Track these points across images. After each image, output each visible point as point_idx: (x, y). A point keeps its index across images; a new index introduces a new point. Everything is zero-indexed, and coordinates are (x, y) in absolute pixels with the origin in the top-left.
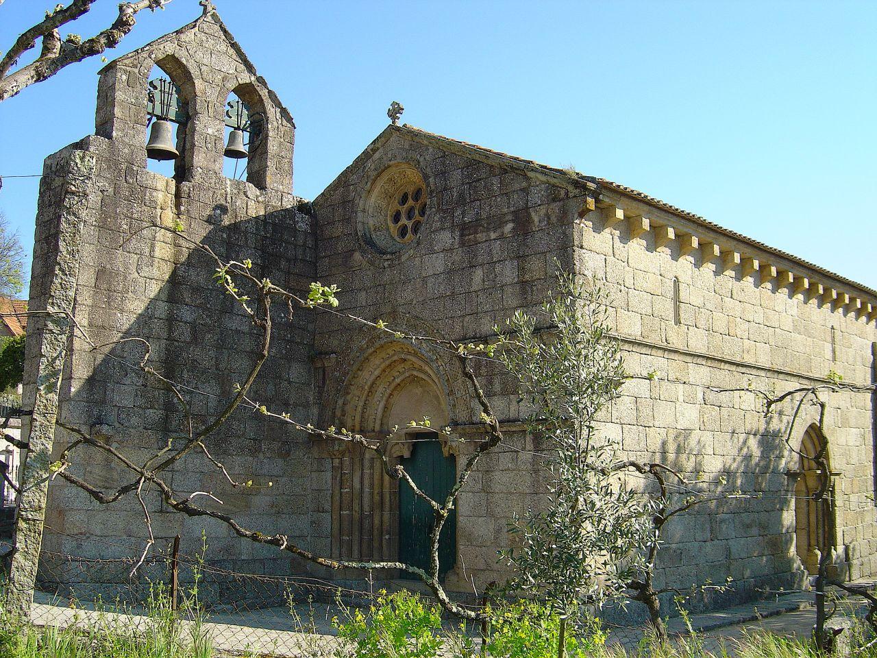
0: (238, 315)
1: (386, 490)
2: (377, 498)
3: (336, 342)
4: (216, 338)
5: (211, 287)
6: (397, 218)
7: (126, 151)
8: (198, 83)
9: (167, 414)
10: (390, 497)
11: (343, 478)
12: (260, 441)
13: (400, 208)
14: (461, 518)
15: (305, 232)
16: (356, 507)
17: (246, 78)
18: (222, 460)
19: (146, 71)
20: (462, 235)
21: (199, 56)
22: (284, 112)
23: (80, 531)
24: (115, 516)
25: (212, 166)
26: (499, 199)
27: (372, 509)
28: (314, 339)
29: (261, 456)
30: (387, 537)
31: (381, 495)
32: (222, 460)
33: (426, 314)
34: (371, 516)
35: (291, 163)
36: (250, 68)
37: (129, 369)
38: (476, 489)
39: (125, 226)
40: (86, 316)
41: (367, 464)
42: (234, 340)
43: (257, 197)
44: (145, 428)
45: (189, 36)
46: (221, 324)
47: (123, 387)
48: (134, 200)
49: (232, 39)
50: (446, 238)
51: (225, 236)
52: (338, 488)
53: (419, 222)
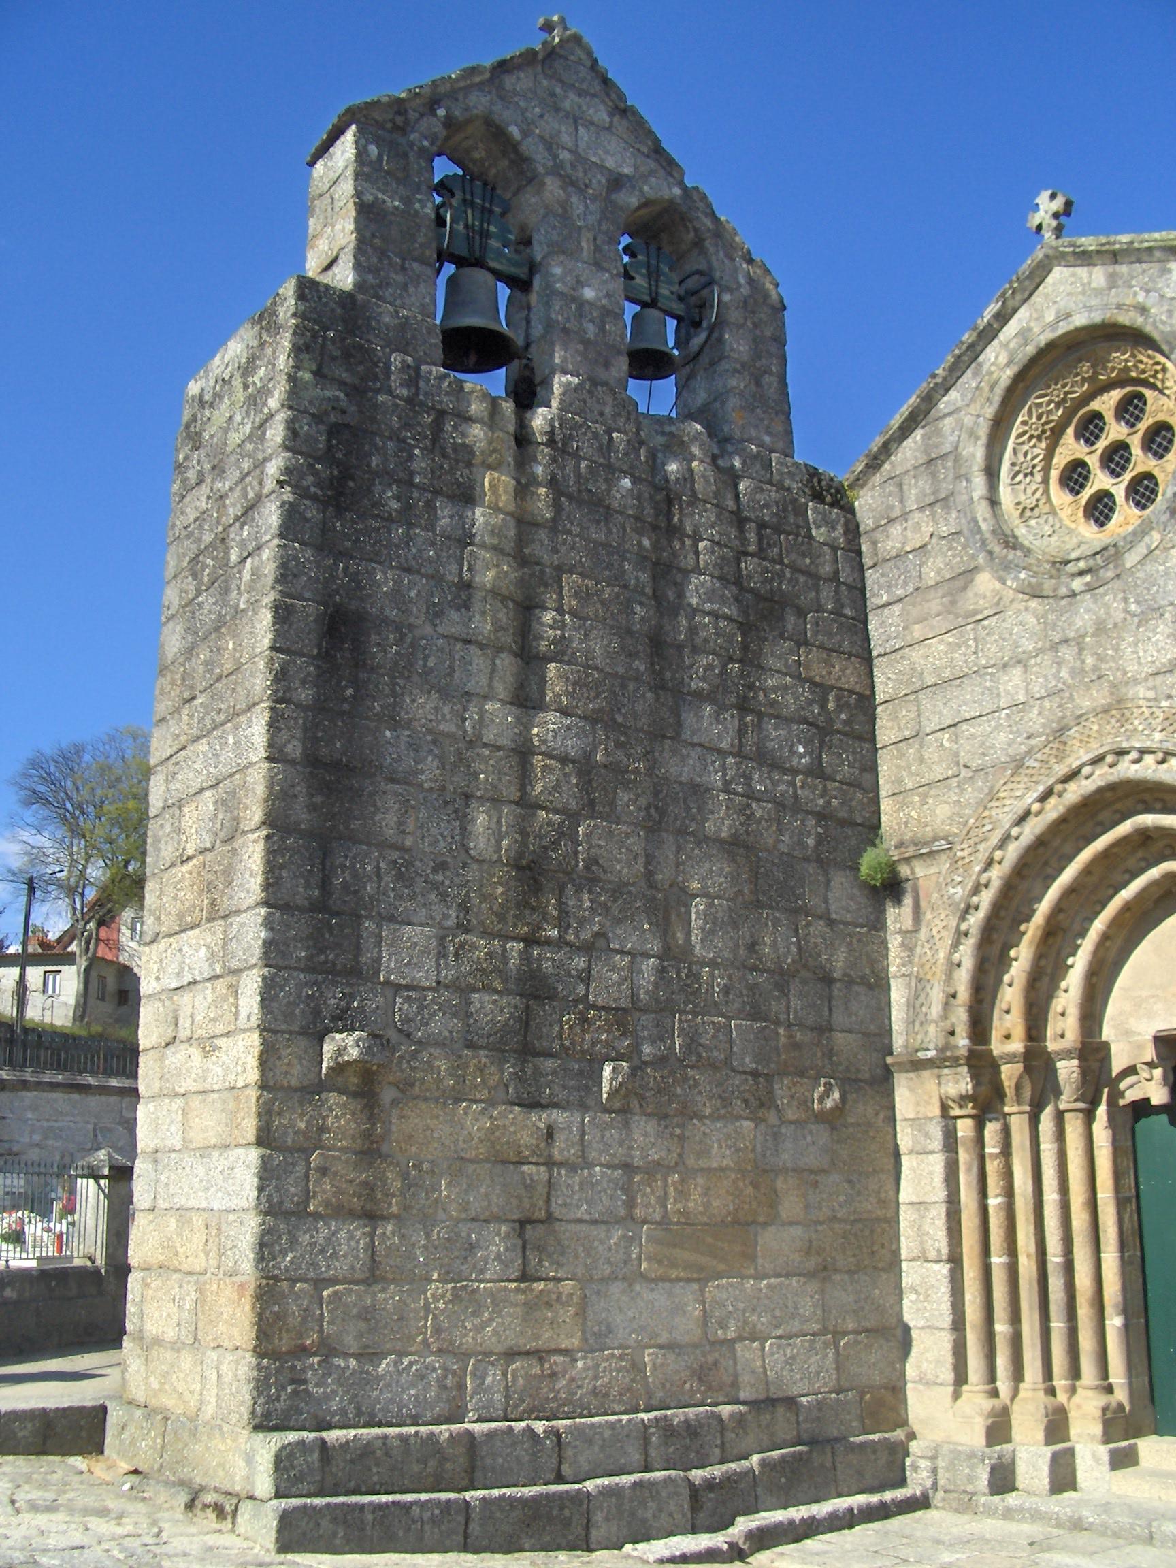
0: (693, 745)
3: (943, 811)
4: (643, 801)
5: (621, 670)
12: (769, 1077)
17: (661, 189)
18: (678, 1131)
29: (772, 1118)
32: (678, 1131)
36: (669, 165)
39: (395, 505)
40: (298, 733)
42: (688, 809)
45: (519, 82)
48: (414, 439)
49: (622, 97)
51: (646, 543)
53: (1149, 476)
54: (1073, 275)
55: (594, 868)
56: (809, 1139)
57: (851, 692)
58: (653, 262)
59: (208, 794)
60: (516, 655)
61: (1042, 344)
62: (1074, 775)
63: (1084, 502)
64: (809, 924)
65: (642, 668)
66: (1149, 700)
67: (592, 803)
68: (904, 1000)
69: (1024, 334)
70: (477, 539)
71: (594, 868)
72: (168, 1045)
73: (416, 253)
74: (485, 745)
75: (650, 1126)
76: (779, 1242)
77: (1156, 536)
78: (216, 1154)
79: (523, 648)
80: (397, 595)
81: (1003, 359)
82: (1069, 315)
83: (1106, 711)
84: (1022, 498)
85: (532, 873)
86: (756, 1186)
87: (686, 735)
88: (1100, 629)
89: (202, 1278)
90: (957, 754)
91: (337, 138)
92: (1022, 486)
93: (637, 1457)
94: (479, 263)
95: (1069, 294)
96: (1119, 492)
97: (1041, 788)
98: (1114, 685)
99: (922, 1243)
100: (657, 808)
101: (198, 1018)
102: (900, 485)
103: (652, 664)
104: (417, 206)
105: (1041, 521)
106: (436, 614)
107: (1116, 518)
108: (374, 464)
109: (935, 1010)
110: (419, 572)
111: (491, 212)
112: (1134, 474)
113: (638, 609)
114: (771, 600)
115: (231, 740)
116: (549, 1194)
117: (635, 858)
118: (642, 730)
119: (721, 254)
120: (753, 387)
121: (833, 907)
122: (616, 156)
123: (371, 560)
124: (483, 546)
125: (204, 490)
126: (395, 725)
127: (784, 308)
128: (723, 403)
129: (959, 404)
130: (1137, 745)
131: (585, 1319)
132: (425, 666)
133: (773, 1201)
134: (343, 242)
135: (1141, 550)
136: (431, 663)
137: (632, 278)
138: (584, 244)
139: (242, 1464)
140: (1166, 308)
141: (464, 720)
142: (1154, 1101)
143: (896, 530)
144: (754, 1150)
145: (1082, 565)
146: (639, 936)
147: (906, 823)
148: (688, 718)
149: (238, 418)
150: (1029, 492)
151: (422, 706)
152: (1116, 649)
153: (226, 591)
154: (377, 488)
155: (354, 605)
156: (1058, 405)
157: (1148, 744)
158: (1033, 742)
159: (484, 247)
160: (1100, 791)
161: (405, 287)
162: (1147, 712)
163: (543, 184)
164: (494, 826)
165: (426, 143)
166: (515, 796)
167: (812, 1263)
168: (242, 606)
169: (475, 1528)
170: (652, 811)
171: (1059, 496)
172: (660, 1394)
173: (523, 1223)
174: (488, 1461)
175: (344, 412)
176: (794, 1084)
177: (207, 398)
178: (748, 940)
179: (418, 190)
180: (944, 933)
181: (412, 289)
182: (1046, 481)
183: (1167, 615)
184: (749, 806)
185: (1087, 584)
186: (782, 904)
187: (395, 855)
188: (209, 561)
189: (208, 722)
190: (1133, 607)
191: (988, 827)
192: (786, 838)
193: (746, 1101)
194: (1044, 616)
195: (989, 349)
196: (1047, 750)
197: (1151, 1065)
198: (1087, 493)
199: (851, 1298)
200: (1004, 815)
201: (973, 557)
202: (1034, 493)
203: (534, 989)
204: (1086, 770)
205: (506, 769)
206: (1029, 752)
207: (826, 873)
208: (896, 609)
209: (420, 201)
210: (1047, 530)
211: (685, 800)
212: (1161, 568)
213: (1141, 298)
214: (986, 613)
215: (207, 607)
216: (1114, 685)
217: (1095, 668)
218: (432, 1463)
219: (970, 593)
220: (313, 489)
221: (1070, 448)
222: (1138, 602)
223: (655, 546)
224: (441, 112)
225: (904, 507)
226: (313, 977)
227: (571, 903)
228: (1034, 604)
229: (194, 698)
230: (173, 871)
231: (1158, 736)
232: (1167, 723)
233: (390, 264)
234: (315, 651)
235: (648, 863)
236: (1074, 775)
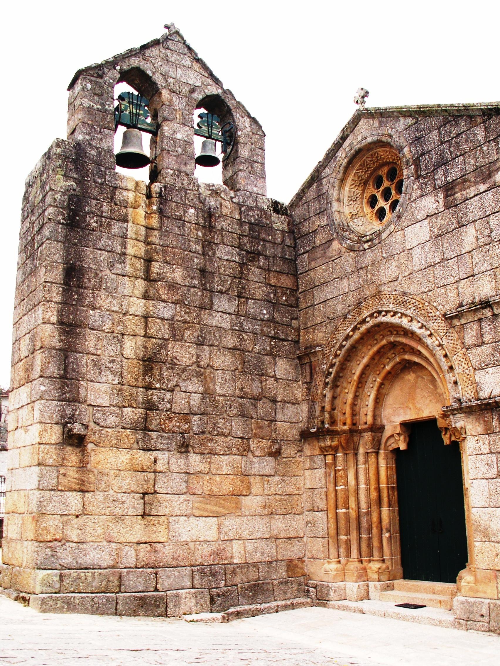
0: (218, 312)
1: (383, 485)
2: (374, 494)
3: (321, 335)
4: (196, 334)
6: (373, 202)
7: (93, 152)
8: (165, 93)
9: (147, 413)
10: (388, 492)
11: (337, 475)
12: (248, 439)
13: (375, 192)
14: (474, 511)
15: (283, 231)
16: (352, 504)
17: (213, 90)
18: (209, 460)
19: (111, 81)
20: (446, 197)
21: (165, 68)
22: (254, 121)
23: (54, 538)
24: (93, 521)
25: (183, 168)
26: (485, 148)
27: (369, 507)
28: (299, 335)
29: (250, 455)
30: (387, 535)
31: (378, 490)
32: (209, 460)
33: (413, 289)
34: (369, 513)
35: (263, 164)
36: (217, 81)
37: (103, 368)
38: (490, 475)
39: (95, 224)
40: (55, 313)
41: (361, 458)
43: (232, 198)
44: (123, 428)
45: (154, 52)
46: (200, 321)
47: (97, 385)
48: (104, 199)
49: (196, 54)
50: (431, 203)
51: (200, 234)
52: (332, 485)
54: (368, 122)
55: (175, 360)
56: (265, 463)
57: (287, 289)
58: (210, 120)
59: (27, 335)
60: (144, 280)
61: (357, 149)
62: (364, 321)
63: (375, 212)
64: (266, 380)
65: (197, 283)
66: (389, 292)
67: (174, 336)
68: (307, 409)
69: (351, 145)
70: (128, 237)
71: (175, 360)
72: (16, 429)
73: (106, 126)
74: (131, 315)
75: (197, 458)
76: (252, 503)
77: (393, 227)
78: (28, 468)
79: (147, 277)
80: (95, 260)
81: (344, 156)
83: (374, 296)
84: (352, 211)
85: (149, 363)
86: (242, 482)
87: (215, 307)
88: (373, 263)
89: (24, 515)
90: (325, 313)
91: (76, 81)
92: (352, 206)
93: (189, 583)
94: (135, 127)
95: (366, 129)
96: (387, 208)
97: (352, 326)
98: (377, 286)
99: (313, 504)
100: (202, 337)
101: (24, 419)
102: (308, 206)
103: (201, 281)
104: (107, 107)
105: (359, 219)
106: (111, 266)
107: (386, 218)
108: (87, 210)
109: (317, 413)
110: (104, 250)
111: (140, 105)
112: (392, 200)
113: (195, 260)
114: (254, 253)
115: (34, 316)
116: (155, 483)
117: (193, 356)
118: (196, 307)
119: (238, 115)
120: (250, 168)
121: (277, 374)
122: (194, 78)
123: (85, 246)
124: (131, 239)
125: (28, 220)
126: (94, 308)
127: (265, 135)
128: (237, 176)
130: (384, 309)
131: (169, 530)
132: (106, 286)
133: (249, 487)
134: (77, 123)
135: (387, 232)
136: (108, 285)
137: (201, 127)
138: (178, 116)
139: (32, 582)
140: (398, 135)
141: (122, 306)
142: (401, 449)
143: (307, 224)
144: (241, 468)
146: (194, 386)
147: (308, 340)
148: (216, 301)
149: (38, 193)
150: (355, 208)
151: (104, 301)
152: (378, 272)
153: (33, 260)
154: (88, 219)
155: (78, 263)
156: (365, 172)
157: (388, 309)
158: (350, 308)
159: (137, 120)
160: (372, 327)
161: (101, 140)
162: (388, 296)
163: (161, 93)
164: (133, 345)
165: (111, 81)
166: (143, 333)
167: (266, 511)
168: (38, 265)
169: (120, 607)
170: (200, 338)
171: (367, 209)
172: (200, 560)
173: (144, 494)
174: (127, 582)
175: (75, 190)
176: (259, 442)
177: (31, 184)
178: (240, 387)
179: (108, 101)
180: (320, 383)
181: (104, 140)
182: (362, 203)
183: (395, 258)
184: (241, 334)
185: (369, 246)
186: (256, 372)
187: (94, 357)
188: (29, 248)
189: (27, 309)
190: (384, 255)
191: (335, 341)
192: (257, 347)
193: (238, 449)
194: (355, 258)
195: (339, 151)
196: (354, 311)
197: (399, 434)
198: (377, 208)
199: (283, 526)
200: (340, 336)
201: (332, 235)
202: (357, 208)
203: (150, 406)
204: (368, 319)
205: (139, 324)
206: (349, 312)
207: (274, 359)
208: (306, 255)
209: (108, 104)
210: (360, 223)
211: (214, 333)
212: (394, 239)
214: (336, 257)
215: (28, 265)
216: (377, 286)
217: (371, 279)
218: (104, 583)
219: (330, 250)
220: (62, 221)
221: (371, 190)
222: (386, 253)
223: (204, 235)
224: (118, 68)
225: (309, 215)
226: (60, 403)
227: (165, 374)
228: (351, 254)
229: (24, 299)
230: (18, 364)
231: (391, 306)
232: (394, 301)
233: (95, 131)
234: (62, 282)
235: (198, 358)
236: (364, 321)
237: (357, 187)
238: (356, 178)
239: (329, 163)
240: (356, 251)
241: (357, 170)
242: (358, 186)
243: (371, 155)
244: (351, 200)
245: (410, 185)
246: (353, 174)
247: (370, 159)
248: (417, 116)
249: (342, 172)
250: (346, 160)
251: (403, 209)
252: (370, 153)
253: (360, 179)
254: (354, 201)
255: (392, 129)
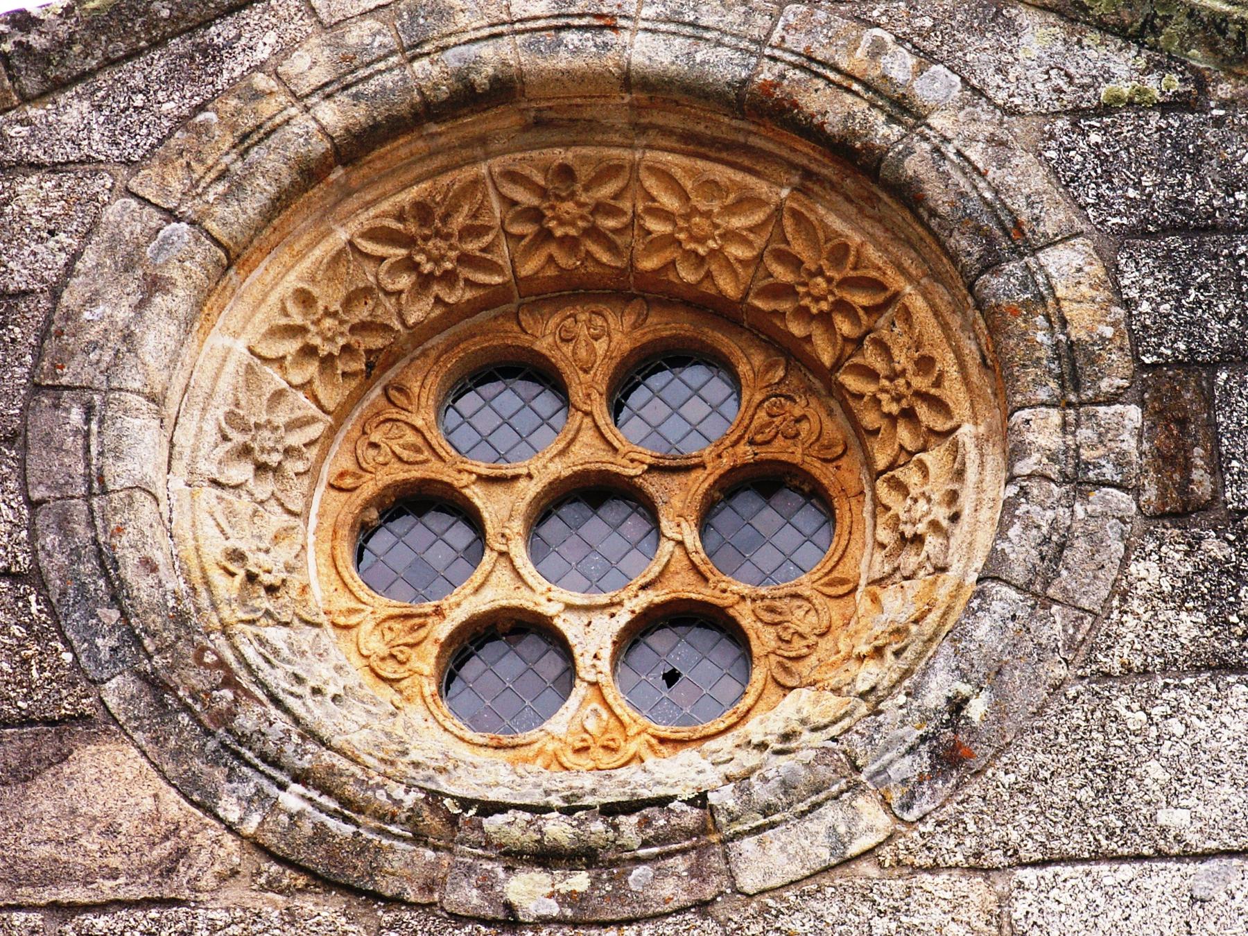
63: (443, 630)
81: (310, 64)
82: (607, 23)
129: (98, 144)
145: (558, 829)
213: (899, 65)
214: (107, 889)
219: (43, 800)
237: (312, 369)
238: (329, 296)
239: (110, 62)
240: (396, 901)
241: (373, 235)
242: (327, 362)
243: (566, 172)
244: (246, 451)
245: (1096, 542)
246: (321, 252)
247: (524, 197)
248: (1197, 57)
249: (261, 191)
250: (331, 114)
251: (999, 710)
252: (561, 155)
253: (362, 313)
254: (261, 468)
255: (927, 58)
